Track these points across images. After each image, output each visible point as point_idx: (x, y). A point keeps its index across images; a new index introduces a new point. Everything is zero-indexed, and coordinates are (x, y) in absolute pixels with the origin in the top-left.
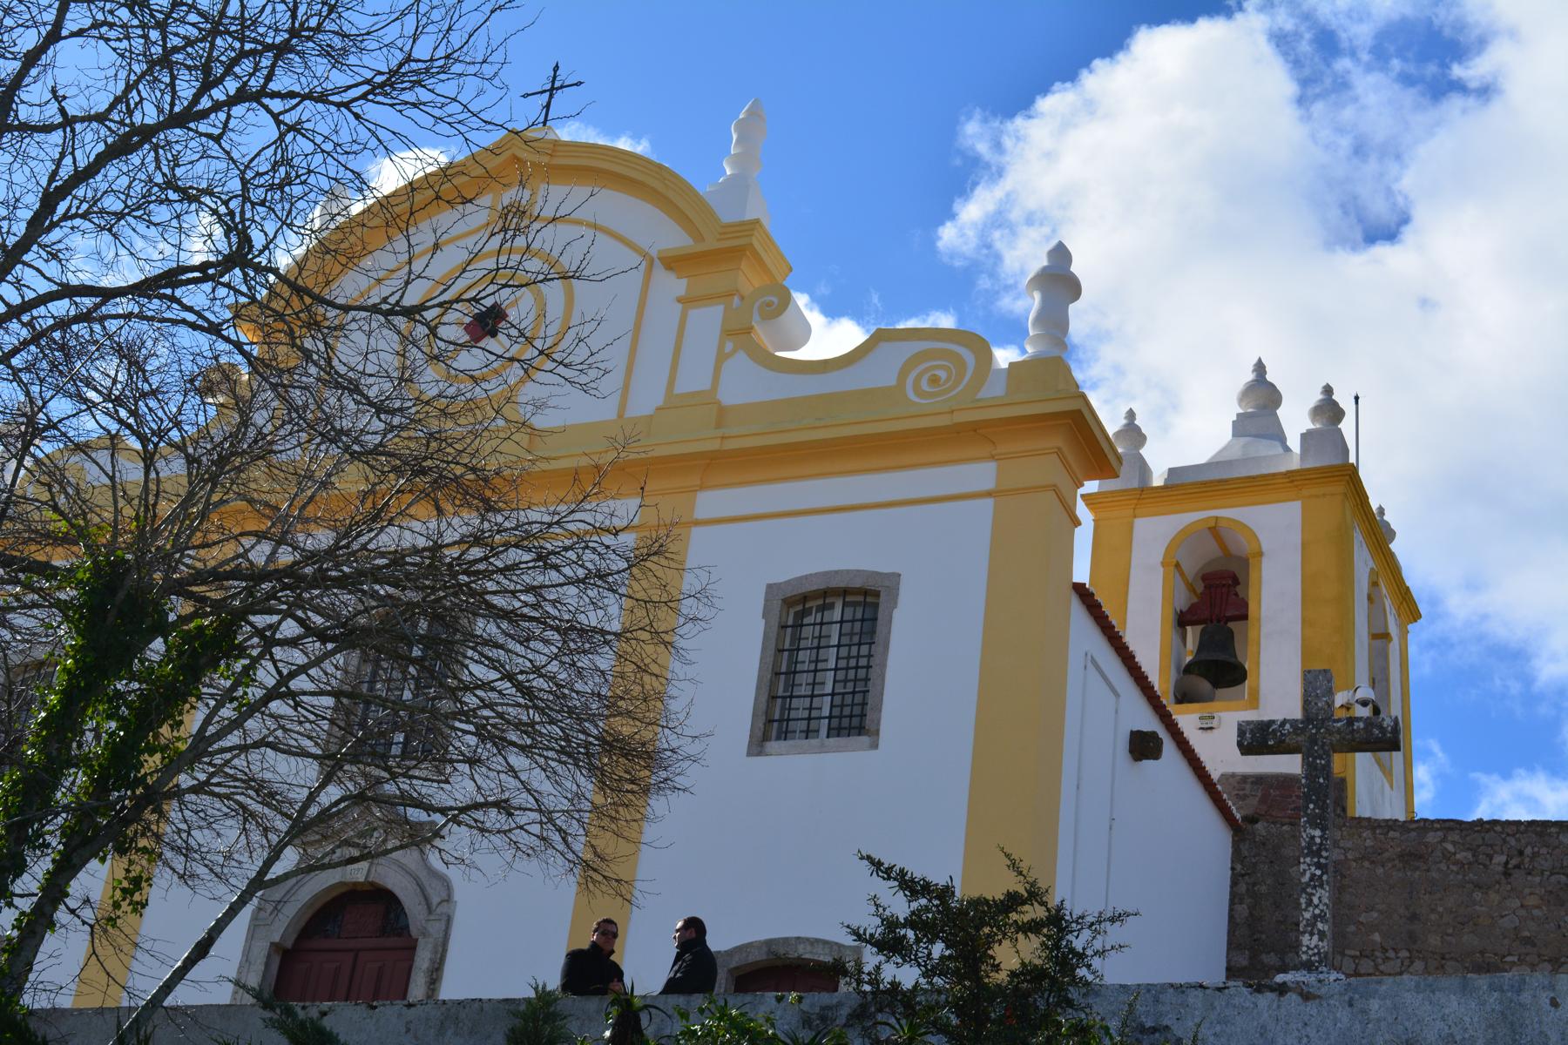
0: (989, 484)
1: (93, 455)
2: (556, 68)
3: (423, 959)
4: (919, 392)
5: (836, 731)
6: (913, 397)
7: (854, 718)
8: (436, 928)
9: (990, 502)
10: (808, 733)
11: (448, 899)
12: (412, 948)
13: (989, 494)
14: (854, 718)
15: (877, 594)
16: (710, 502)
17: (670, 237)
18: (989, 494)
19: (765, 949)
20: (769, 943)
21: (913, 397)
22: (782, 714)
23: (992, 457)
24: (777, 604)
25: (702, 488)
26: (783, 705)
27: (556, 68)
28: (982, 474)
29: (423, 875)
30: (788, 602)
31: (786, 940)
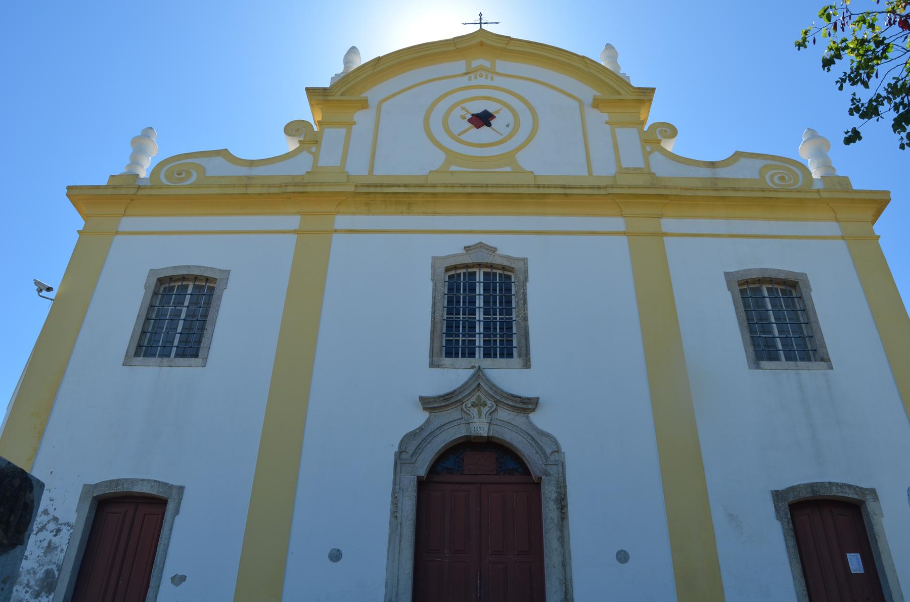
0: (296, 226)
1: (760, 163)
2: (481, 15)
3: (549, 491)
4: (772, 177)
5: (181, 354)
6: (768, 181)
7: (192, 346)
8: (553, 470)
9: (295, 236)
10: (165, 354)
11: (558, 451)
12: (538, 485)
13: (336, 231)
14: (192, 346)
15: (214, 280)
16: (342, 221)
17: (588, 93)
18: (295, 232)
19: (809, 490)
20: (812, 485)
21: (768, 181)
22: (149, 342)
23: (298, 213)
24: (154, 281)
25: (338, 213)
26: (150, 337)
27: (481, 15)
28: (293, 222)
29: (533, 433)
30: (160, 281)
31: (822, 484)
